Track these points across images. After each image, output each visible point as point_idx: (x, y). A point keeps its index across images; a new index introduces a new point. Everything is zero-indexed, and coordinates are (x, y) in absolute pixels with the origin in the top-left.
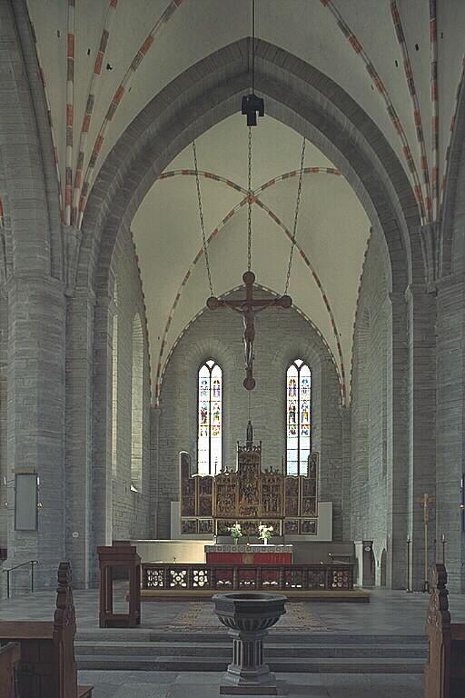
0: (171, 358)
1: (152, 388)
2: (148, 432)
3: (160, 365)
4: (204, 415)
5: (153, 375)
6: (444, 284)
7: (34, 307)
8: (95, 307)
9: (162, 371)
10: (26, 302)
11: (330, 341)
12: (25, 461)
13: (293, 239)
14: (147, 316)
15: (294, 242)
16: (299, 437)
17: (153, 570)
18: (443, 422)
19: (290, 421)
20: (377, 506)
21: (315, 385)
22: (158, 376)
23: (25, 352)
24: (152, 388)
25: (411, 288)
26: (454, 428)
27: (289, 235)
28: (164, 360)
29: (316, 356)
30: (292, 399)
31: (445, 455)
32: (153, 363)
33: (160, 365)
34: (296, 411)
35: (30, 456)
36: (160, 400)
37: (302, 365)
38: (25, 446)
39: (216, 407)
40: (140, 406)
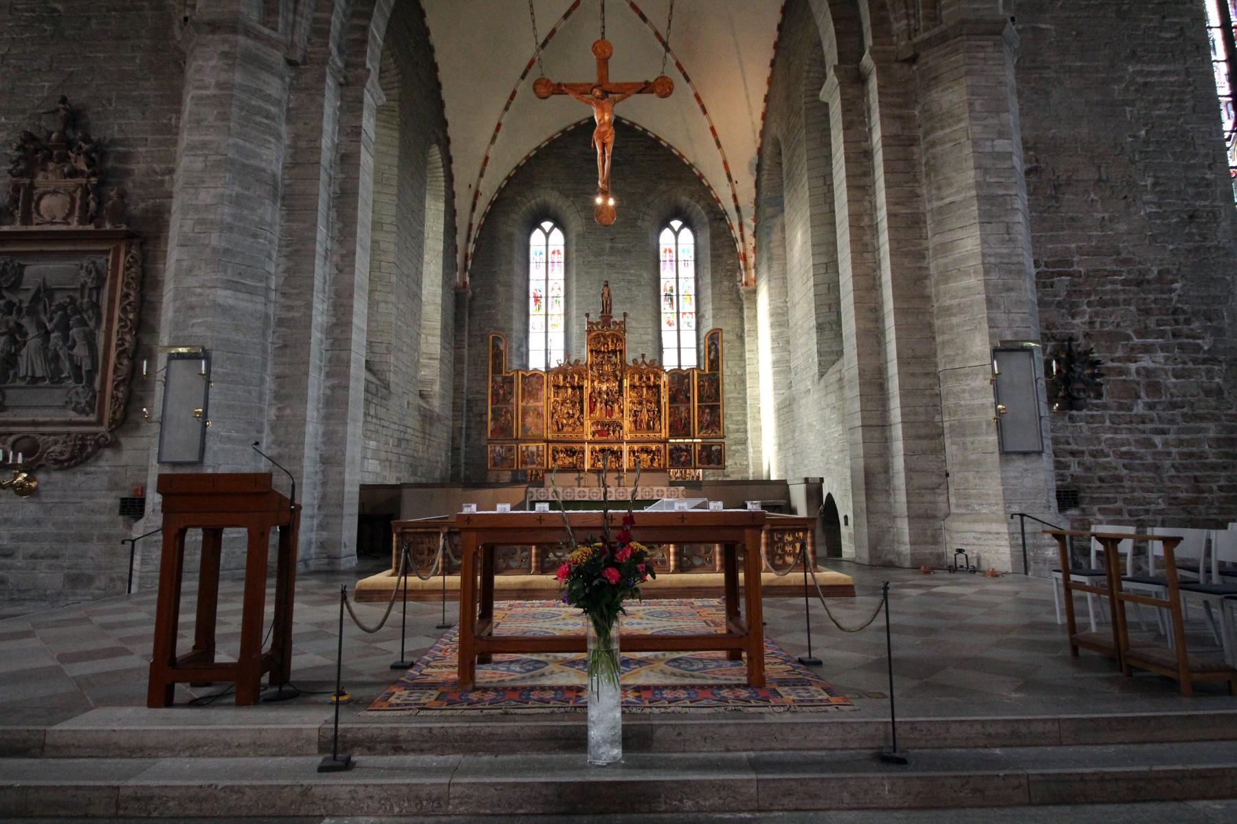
0: (488, 216)
1: (459, 258)
2: (451, 322)
3: (470, 225)
4: (537, 299)
5: (460, 240)
6: (928, 43)
7: (225, 71)
8: (341, 85)
9: (475, 233)
10: (213, 63)
11: (722, 192)
12: (186, 333)
13: (665, 45)
14: (452, 153)
15: (668, 50)
16: (679, 330)
17: (783, 532)
18: (946, 265)
19: (665, 305)
20: (810, 425)
21: (701, 256)
22: (468, 240)
23: (204, 145)
24: (459, 258)
25: (871, 53)
26: (967, 274)
27: (660, 39)
28: (477, 219)
29: (698, 210)
30: (667, 273)
31: (955, 320)
32: (461, 222)
33: (470, 225)
34: (674, 293)
35: (200, 325)
36: (471, 276)
37: (681, 228)
38: (192, 308)
39: (556, 287)
40: (439, 280)
